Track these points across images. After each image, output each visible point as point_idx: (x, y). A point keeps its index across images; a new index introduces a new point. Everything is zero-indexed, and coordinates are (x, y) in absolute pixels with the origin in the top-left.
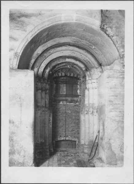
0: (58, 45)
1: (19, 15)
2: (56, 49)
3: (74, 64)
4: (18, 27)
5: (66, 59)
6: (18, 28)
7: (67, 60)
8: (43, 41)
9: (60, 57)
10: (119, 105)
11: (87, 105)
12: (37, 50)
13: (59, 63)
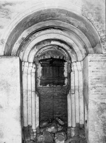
0: (22, 103)
1: (4, 3)
2: (41, 33)
4: (3, 15)
6: (3, 16)
7: (53, 43)
9: (47, 40)
10: (101, 88)
12: (22, 34)
13: (44, 45)
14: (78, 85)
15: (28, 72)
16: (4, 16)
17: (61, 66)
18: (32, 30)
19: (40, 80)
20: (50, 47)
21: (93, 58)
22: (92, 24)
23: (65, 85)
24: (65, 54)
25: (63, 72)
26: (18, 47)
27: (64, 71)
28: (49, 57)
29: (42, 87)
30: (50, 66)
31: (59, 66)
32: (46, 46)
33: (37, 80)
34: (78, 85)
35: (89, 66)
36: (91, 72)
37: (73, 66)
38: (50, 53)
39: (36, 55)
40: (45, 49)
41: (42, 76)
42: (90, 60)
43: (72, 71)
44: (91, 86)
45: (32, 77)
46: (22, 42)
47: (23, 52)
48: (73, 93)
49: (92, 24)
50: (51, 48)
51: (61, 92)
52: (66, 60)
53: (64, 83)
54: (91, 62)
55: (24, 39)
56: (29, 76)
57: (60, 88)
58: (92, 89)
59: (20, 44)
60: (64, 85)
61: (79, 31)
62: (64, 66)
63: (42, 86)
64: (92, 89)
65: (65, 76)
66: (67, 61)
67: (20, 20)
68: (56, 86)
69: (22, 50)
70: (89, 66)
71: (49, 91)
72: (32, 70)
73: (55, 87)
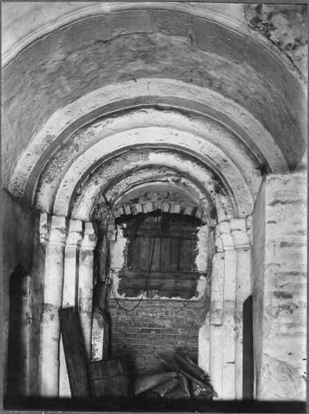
7: (154, 158)
9: (132, 149)
11: (219, 306)
14: (236, 296)
21: (285, 191)
22: (290, 58)
23: (197, 296)
24: (201, 200)
25: (193, 255)
26: (31, 167)
27: (197, 253)
28: (149, 208)
29: (123, 300)
33: (111, 277)
34: (234, 296)
35: (269, 222)
36: (275, 246)
37: (221, 234)
38: (155, 197)
39: (99, 197)
42: (272, 200)
43: (217, 252)
44: (276, 302)
47: (54, 183)
48: (219, 323)
49: (290, 58)
51: (181, 317)
52: (204, 220)
53: (193, 292)
54: (279, 207)
55: (54, 140)
56: (71, 262)
57: (181, 305)
58: (277, 313)
61: (243, 114)
62: (196, 239)
63: (126, 297)
64: (277, 313)
65: (199, 269)
66: (208, 221)
68: (167, 298)
69: (47, 179)
70: (267, 220)
71: (146, 311)
73: (163, 301)
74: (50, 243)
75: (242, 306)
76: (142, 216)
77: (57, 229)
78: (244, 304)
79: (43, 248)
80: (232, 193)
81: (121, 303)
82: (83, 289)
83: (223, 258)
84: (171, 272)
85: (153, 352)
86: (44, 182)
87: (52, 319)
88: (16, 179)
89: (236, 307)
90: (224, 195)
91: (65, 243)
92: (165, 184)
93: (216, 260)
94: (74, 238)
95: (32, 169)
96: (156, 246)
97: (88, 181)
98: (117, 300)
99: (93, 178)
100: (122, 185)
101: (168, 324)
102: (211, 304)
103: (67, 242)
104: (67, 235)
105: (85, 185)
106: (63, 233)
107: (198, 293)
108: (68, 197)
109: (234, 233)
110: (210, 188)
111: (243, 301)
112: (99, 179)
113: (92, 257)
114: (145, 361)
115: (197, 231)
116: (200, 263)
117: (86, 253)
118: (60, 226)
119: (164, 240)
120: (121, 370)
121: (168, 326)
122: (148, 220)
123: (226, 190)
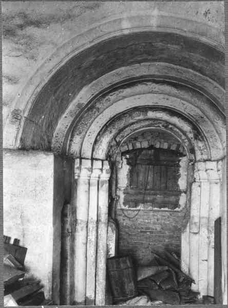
3: (167, 124)
5: (147, 111)
7: (151, 114)
8: (88, 76)
9: (136, 109)
11: (196, 220)
12: (78, 97)
13: (131, 121)
14: (209, 215)
15: (91, 181)
16: (22, 53)
17: (172, 166)
18: (101, 87)
19: (124, 193)
20: (147, 123)
23: (179, 208)
24: (183, 140)
25: (176, 177)
26: (67, 126)
27: (179, 176)
28: (145, 145)
29: (127, 210)
30: (146, 163)
31: (167, 166)
32: (137, 122)
40: (135, 128)
41: (128, 186)
43: (195, 181)
45: (100, 192)
46: (77, 113)
48: (197, 232)
50: (149, 126)
53: (176, 205)
56: (94, 189)
57: (168, 214)
59: (74, 117)
60: (177, 207)
61: (215, 87)
62: (179, 166)
63: (129, 207)
67: (61, 62)
72: (101, 176)
74: (81, 178)
75: (214, 222)
76: (142, 149)
77: (86, 168)
78: (215, 222)
79: (76, 182)
80: (207, 140)
81: (126, 213)
82: (101, 207)
83: (200, 186)
84: (160, 190)
85: (148, 247)
86: (76, 134)
87: (82, 230)
88: (57, 134)
89: (208, 222)
90: (201, 141)
91: (90, 177)
92: (158, 128)
93: (194, 186)
94: (96, 173)
95: (68, 127)
96: (149, 177)
97: (105, 131)
98: (122, 210)
99: (109, 129)
100: (128, 130)
101: (158, 228)
102: (191, 219)
103: (92, 176)
104: (92, 172)
105: (103, 134)
106: (89, 171)
107: (180, 205)
108: (91, 144)
109: (208, 171)
110: (191, 136)
111: (215, 220)
112: (112, 129)
113: (107, 185)
114: (144, 255)
115: (179, 161)
116: (182, 183)
117: (103, 182)
118: (87, 167)
119: (156, 167)
120: (129, 265)
121: (159, 229)
122: (144, 152)
123: (202, 137)
